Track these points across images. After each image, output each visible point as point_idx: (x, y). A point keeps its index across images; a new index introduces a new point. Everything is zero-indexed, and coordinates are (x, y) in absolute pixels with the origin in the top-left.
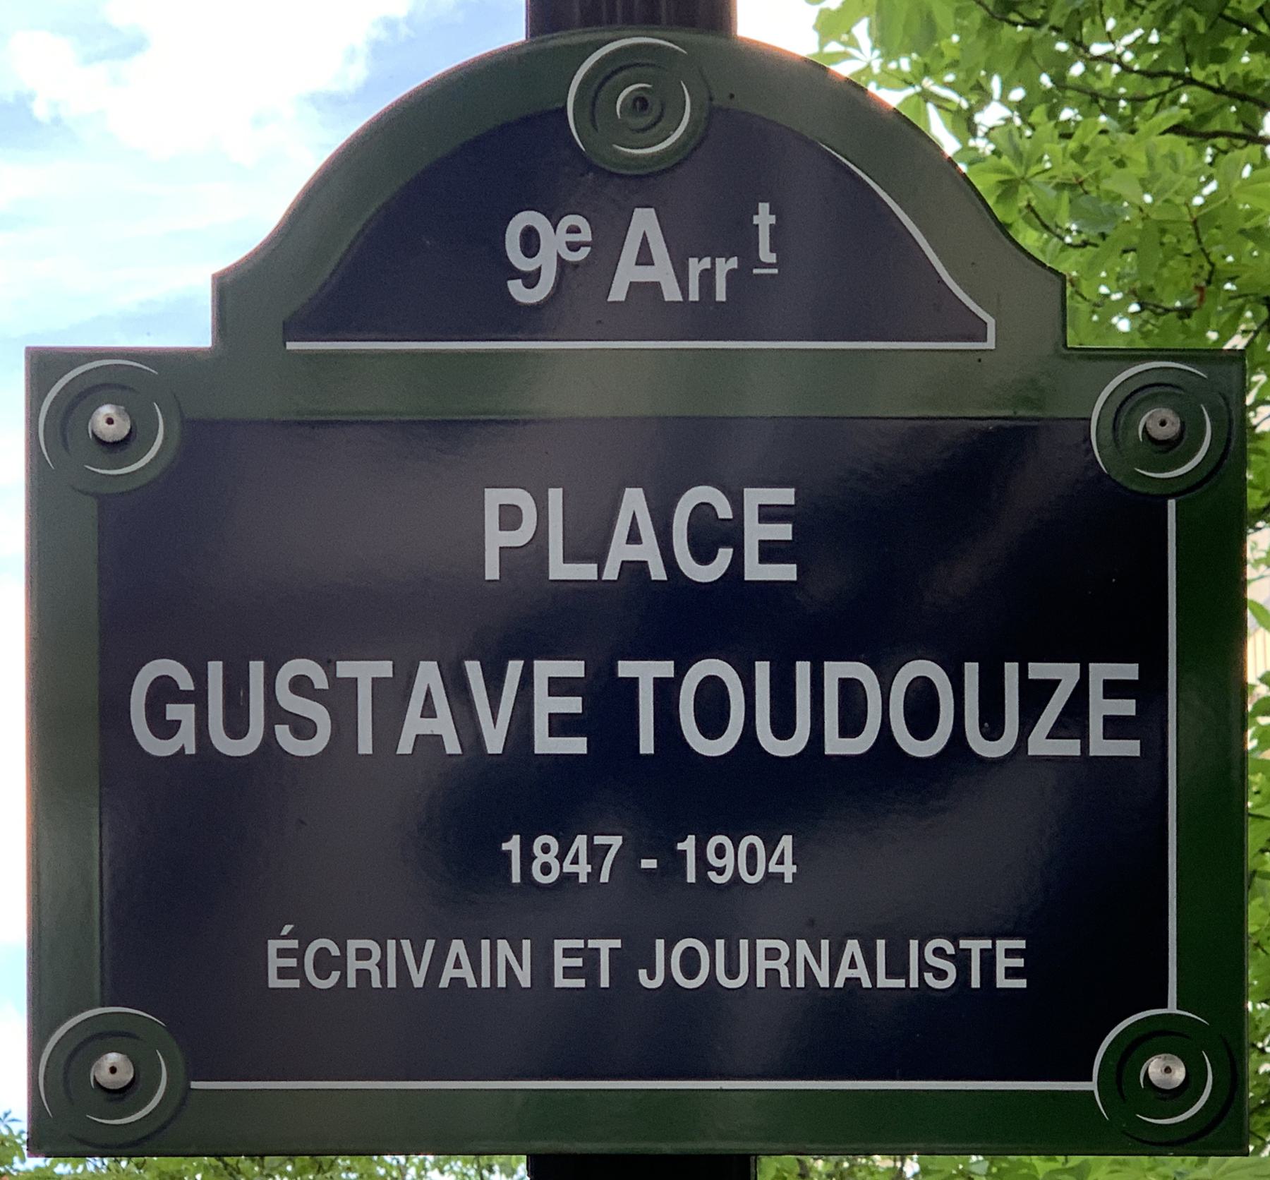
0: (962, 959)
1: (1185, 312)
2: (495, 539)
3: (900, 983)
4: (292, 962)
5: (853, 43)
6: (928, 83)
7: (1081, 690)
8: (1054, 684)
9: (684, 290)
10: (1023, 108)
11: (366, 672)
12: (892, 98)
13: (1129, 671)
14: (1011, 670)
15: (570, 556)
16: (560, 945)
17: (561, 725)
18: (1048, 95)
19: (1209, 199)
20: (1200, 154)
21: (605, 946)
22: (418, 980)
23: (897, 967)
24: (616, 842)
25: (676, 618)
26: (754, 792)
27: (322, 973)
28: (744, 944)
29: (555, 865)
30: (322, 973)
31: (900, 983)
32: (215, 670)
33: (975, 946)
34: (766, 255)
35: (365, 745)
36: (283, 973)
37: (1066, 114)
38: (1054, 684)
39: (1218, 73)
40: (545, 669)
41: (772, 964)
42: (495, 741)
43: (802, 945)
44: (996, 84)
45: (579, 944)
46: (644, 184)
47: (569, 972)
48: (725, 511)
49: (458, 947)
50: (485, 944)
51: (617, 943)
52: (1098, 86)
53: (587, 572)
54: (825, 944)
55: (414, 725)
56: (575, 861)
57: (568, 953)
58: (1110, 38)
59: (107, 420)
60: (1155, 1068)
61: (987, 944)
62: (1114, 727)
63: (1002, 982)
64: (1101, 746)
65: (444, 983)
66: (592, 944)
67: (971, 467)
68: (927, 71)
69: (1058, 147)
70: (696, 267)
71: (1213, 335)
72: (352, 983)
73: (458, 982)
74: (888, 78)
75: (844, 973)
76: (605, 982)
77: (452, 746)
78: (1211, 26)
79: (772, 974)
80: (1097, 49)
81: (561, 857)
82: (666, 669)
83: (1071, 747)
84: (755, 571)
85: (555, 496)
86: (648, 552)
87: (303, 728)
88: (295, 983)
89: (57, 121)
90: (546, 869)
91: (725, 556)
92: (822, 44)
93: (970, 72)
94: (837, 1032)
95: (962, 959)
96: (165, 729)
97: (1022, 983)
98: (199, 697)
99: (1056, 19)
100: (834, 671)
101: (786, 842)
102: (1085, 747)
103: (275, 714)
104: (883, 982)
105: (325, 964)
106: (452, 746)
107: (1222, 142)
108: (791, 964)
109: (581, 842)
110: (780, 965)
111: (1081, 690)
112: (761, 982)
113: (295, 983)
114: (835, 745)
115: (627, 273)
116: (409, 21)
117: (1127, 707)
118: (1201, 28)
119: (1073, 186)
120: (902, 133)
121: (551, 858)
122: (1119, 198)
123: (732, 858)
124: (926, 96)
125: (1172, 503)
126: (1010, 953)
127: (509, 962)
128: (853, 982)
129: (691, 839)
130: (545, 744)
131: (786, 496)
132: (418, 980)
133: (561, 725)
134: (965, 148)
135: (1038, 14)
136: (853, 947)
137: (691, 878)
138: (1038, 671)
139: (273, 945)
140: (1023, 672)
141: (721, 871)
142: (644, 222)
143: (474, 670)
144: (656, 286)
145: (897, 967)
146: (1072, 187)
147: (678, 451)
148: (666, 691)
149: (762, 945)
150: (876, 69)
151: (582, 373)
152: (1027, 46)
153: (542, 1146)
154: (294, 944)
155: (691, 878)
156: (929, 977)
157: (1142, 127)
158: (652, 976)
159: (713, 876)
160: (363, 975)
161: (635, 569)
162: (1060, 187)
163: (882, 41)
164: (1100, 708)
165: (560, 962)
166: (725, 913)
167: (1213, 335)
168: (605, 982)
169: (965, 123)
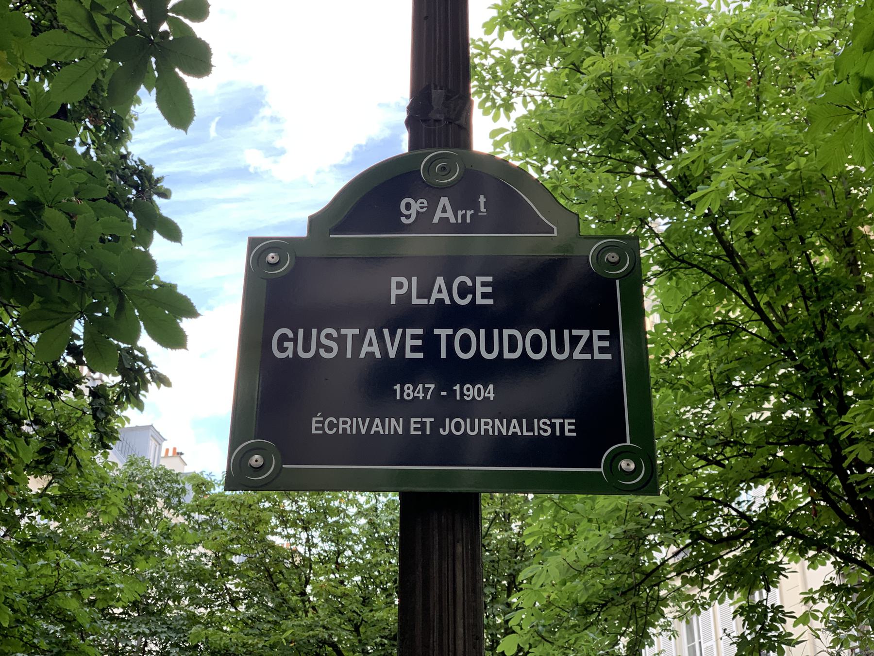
0: (553, 426)
1: (614, 222)
2: (394, 292)
3: (531, 434)
4: (321, 425)
5: (504, 149)
6: (528, 159)
7: (590, 338)
8: (581, 337)
9: (456, 219)
10: (558, 166)
11: (350, 332)
12: (517, 163)
13: (607, 333)
14: (566, 332)
15: (419, 297)
16: (412, 420)
17: (414, 349)
18: (566, 162)
19: (619, 191)
20: (615, 178)
21: (428, 421)
22: (363, 431)
23: (530, 428)
24: (433, 386)
25: (451, 316)
26: (479, 370)
27: (330, 429)
28: (476, 420)
29: (412, 394)
30: (330, 429)
31: (531, 434)
32: (301, 332)
33: (557, 421)
34: (483, 209)
35: (349, 355)
36: (317, 429)
37: (572, 167)
38: (581, 337)
39: (620, 156)
40: (409, 332)
41: (486, 427)
42: (392, 354)
43: (497, 421)
44: (549, 160)
45: (420, 420)
46: (443, 190)
47: (415, 429)
48: (470, 283)
49: (377, 420)
50: (387, 419)
51: (432, 420)
52: (581, 160)
53: (424, 302)
54: (505, 420)
55: (365, 349)
56: (418, 392)
57: (415, 423)
58: (585, 146)
59: (272, 257)
60: (623, 464)
61: (562, 421)
62: (602, 350)
63: (567, 434)
64: (598, 356)
65: (372, 432)
66: (424, 420)
67: (546, 270)
68: (527, 156)
69: (570, 177)
70: (460, 213)
71: (623, 229)
72: (340, 432)
73: (377, 432)
74: (514, 158)
75: (512, 430)
76: (428, 433)
77: (378, 355)
78: (616, 143)
79: (486, 430)
80: (581, 150)
81: (414, 391)
82: (450, 331)
83: (588, 357)
84: (479, 301)
85: (414, 279)
86: (445, 296)
87: (329, 350)
88: (321, 432)
89: (256, 173)
90: (408, 395)
91: (470, 297)
92: (495, 149)
93: (541, 156)
94: (505, 450)
95: (553, 426)
96: (282, 349)
97: (574, 434)
98: (295, 340)
99: (567, 142)
100: (506, 332)
101: (491, 387)
102: (592, 356)
103: (319, 345)
104: (525, 433)
105: (331, 426)
106: (378, 355)
107: (622, 175)
108: (493, 427)
109: (420, 386)
110: (489, 427)
111: (590, 338)
112: (482, 433)
113: (321, 432)
114: (507, 355)
115: (438, 215)
116: (366, 146)
117: (606, 344)
118: (613, 144)
119: (576, 187)
120: (521, 173)
121: (410, 391)
122: (591, 190)
123: (472, 392)
124: (527, 163)
125: (617, 281)
126: (569, 424)
127: (395, 426)
128: (515, 433)
129: (458, 386)
130: (409, 355)
131: (490, 279)
132: (363, 431)
133: (414, 349)
134: (540, 177)
135: (562, 141)
136: (514, 421)
137: (458, 398)
138: (575, 332)
139: (314, 419)
140: (570, 333)
141: (468, 396)
142: (444, 201)
143: (386, 332)
144: (448, 219)
145: (530, 428)
146: (575, 187)
147: (451, 267)
148: (450, 339)
149: (483, 420)
150: (511, 155)
151: (419, 244)
152: (559, 149)
153: (405, 489)
154: (321, 419)
155: (458, 398)
156: (541, 432)
157: (597, 171)
158: (444, 431)
159: (465, 397)
160: (344, 429)
161: (440, 301)
162: (571, 187)
163: (513, 148)
164: (597, 344)
165: (413, 426)
166: (468, 409)
167: (623, 229)
168: (428, 433)
169: (540, 170)
